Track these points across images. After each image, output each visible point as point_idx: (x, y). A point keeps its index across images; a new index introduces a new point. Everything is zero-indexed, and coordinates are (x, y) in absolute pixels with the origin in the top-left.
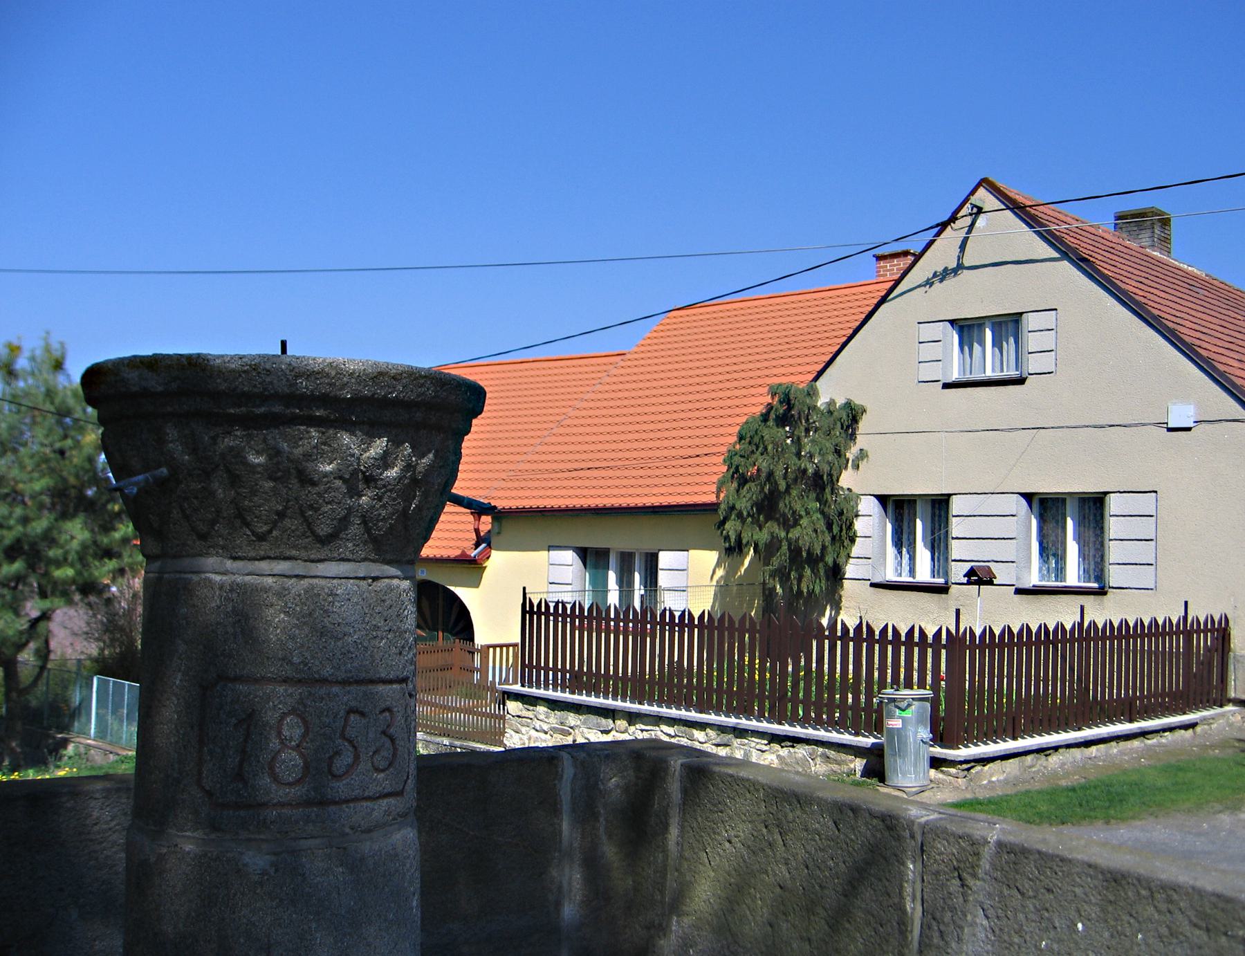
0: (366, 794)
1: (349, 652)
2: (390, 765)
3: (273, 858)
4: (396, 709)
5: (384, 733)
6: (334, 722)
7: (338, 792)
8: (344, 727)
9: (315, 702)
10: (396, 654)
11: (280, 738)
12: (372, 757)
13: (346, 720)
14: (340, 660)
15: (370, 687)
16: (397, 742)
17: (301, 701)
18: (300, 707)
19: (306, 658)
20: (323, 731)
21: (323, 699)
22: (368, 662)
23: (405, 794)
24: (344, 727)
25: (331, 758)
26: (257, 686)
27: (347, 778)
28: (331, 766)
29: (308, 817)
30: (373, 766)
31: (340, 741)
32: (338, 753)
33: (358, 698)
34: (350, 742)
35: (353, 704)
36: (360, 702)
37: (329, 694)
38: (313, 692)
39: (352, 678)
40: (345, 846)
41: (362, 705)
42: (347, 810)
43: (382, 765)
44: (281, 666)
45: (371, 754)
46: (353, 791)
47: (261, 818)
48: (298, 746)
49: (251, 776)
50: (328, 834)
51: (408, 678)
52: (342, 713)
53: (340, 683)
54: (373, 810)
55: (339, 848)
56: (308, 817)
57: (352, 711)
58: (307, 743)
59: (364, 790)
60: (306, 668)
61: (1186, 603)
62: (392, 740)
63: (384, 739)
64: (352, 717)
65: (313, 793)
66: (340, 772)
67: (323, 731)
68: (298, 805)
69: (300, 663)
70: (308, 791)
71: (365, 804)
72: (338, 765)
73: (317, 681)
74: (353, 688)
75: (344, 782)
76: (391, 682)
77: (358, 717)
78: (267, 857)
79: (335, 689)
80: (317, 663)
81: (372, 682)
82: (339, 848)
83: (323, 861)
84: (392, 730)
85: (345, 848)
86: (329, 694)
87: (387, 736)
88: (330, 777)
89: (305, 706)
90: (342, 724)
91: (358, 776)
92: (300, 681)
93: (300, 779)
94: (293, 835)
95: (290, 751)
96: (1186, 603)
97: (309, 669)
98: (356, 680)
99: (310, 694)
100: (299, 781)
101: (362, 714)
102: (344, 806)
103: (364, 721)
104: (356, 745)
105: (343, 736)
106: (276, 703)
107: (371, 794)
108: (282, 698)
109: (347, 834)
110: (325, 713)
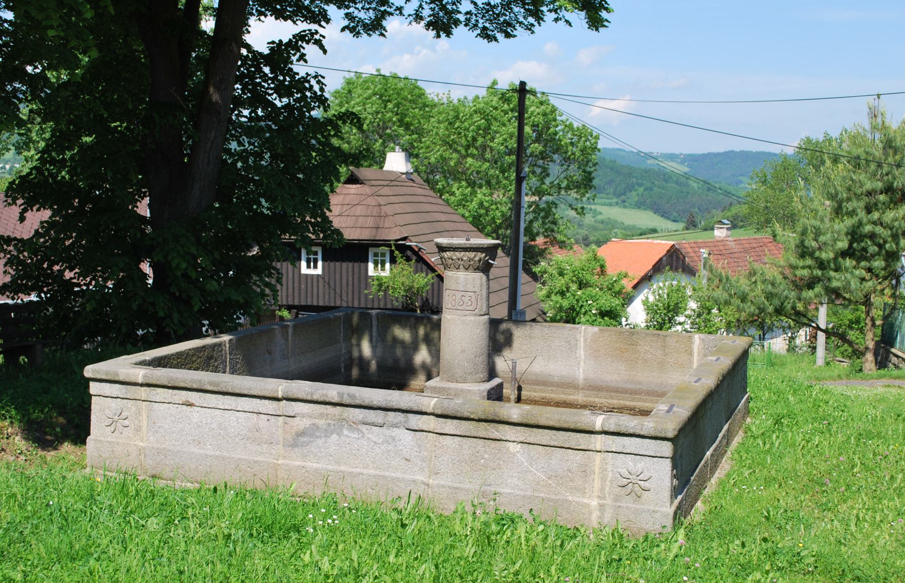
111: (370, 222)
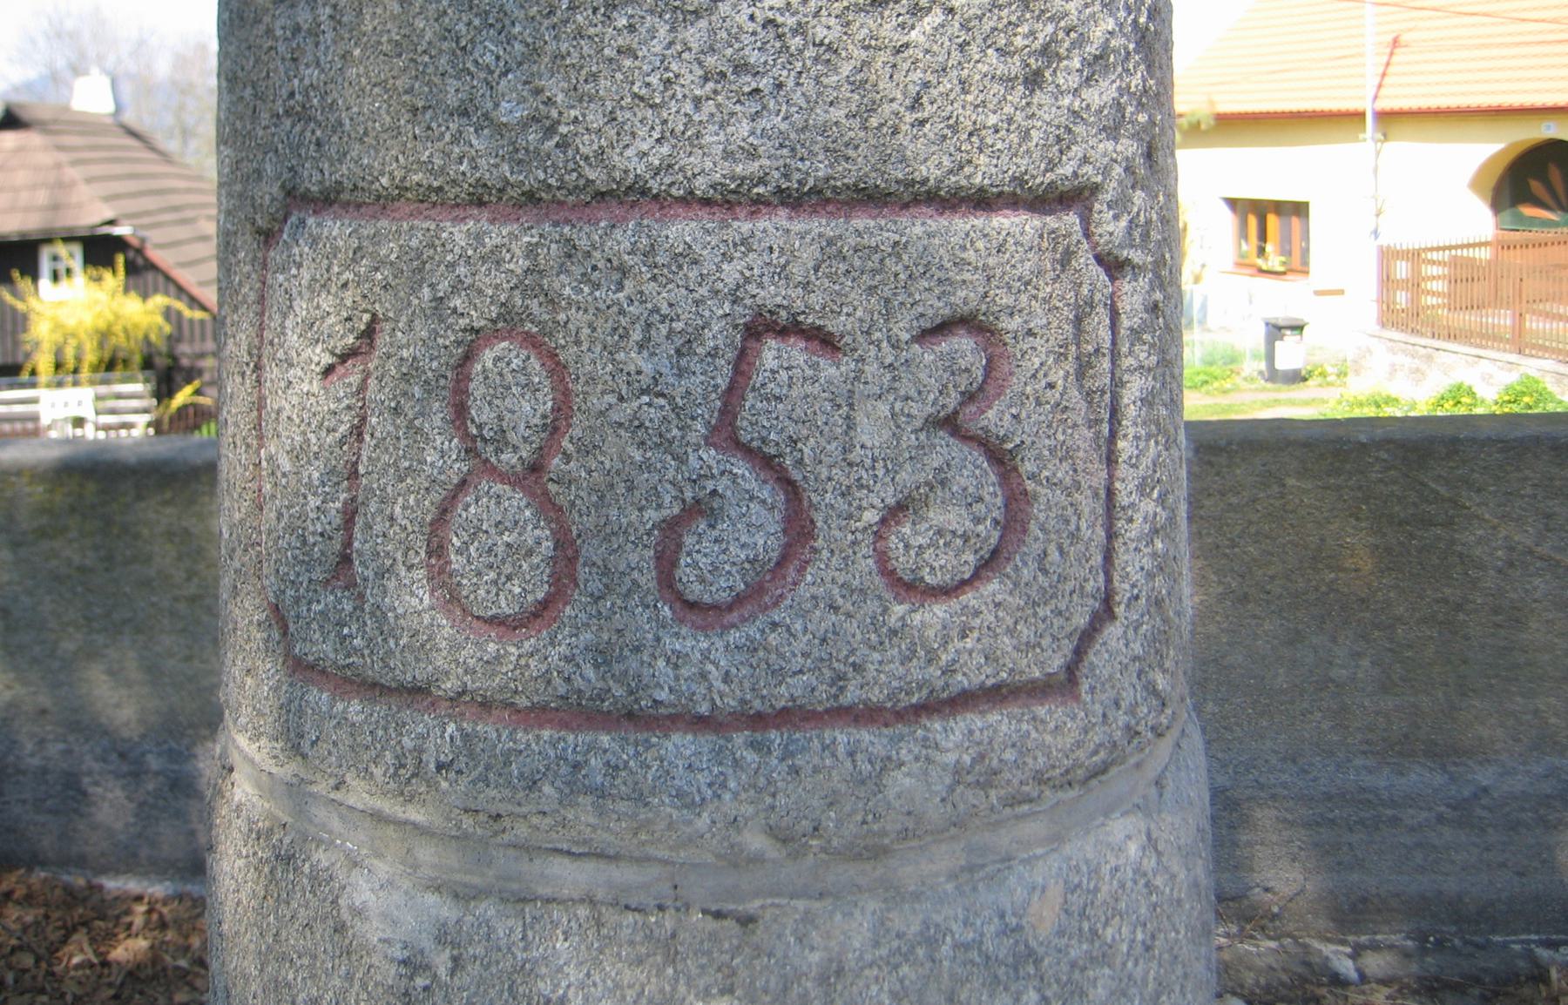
0: (851, 695)
1: (741, 67)
2: (990, 563)
3: (447, 911)
4: (1013, 324)
5: (949, 423)
6: (681, 373)
7: (704, 675)
8: (733, 393)
9: (596, 286)
10: (1008, 81)
11: (466, 435)
12: (879, 533)
13: (743, 363)
14: (697, 102)
15: (860, 222)
16: (1029, 467)
17: (533, 281)
18: (534, 305)
19: (549, 102)
20: (629, 408)
21: (624, 271)
22: (838, 113)
23: (1085, 686)
24: (733, 393)
25: (672, 528)
26: (384, 223)
27: (753, 617)
28: (674, 564)
29: (576, 766)
30: (886, 570)
31: (709, 455)
32: (700, 509)
33: (797, 271)
34: (767, 463)
35: (771, 295)
36: (806, 285)
37: (652, 250)
38: (583, 243)
39: (762, 181)
40: (753, 906)
41: (816, 300)
42: (750, 756)
43: (942, 565)
44: (456, 140)
45: (871, 516)
46: (779, 674)
47: (408, 742)
48: (535, 468)
49: (370, 573)
50: (664, 853)
51: (1095, 189)
52: (717, 335)
53: (707, 202)
54: (888, 764)
55: (718, 915)
56: (576, 766)
57: (761, 326)
58: (567, 458)
59: (840, 677)
60: (551, 143)
61: (1341, 292)
62: (1000, 457)
63: (946, 448)
64: (771, 353)
65: (590, 672)
66: (719, 590)
67: (629, 408)
68: (538, 714)
69: (525, 124)
70: (569, 659)
71: (841, 738)
72: (703, 562)
73: (601, 196)
74: (772, 226)
75: (734, 636)
76: (983, 201)
77: (796, 352)
78: (431, 899)
79: (681, 230)
80: (595, 119)
81: (868, 198)
82: (718, 915)
83: (640, 961)
84: (994, 418)
85: (747, 921)
86: (652, 250)
87: (967, 438)
88: (666, 611)
89: (552, 301)
90: (722, 382)
91: (804, 614)
92: (531, 198)
93: (545, 605)
94: (522, 830)
95: (498, 488)
96: (1341, 292)
97: (563, 145)
98: (779, 191)
99: (570, 250)
100: (540, 613)
101: (824, 341)
102: (739, 738)
103: (829, 370)
104: (796, 475)
105: (725, 434)
106: (444, 286)
107: (876, 695)
108: (462, 270)
109: (757, 859)
110: (636, 335)
111: (42, 197)
